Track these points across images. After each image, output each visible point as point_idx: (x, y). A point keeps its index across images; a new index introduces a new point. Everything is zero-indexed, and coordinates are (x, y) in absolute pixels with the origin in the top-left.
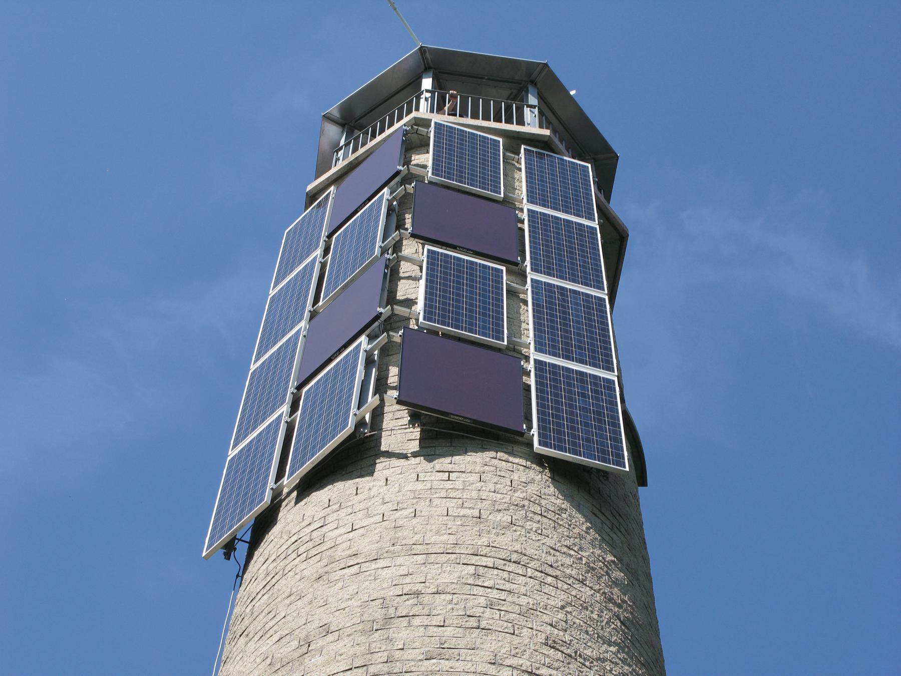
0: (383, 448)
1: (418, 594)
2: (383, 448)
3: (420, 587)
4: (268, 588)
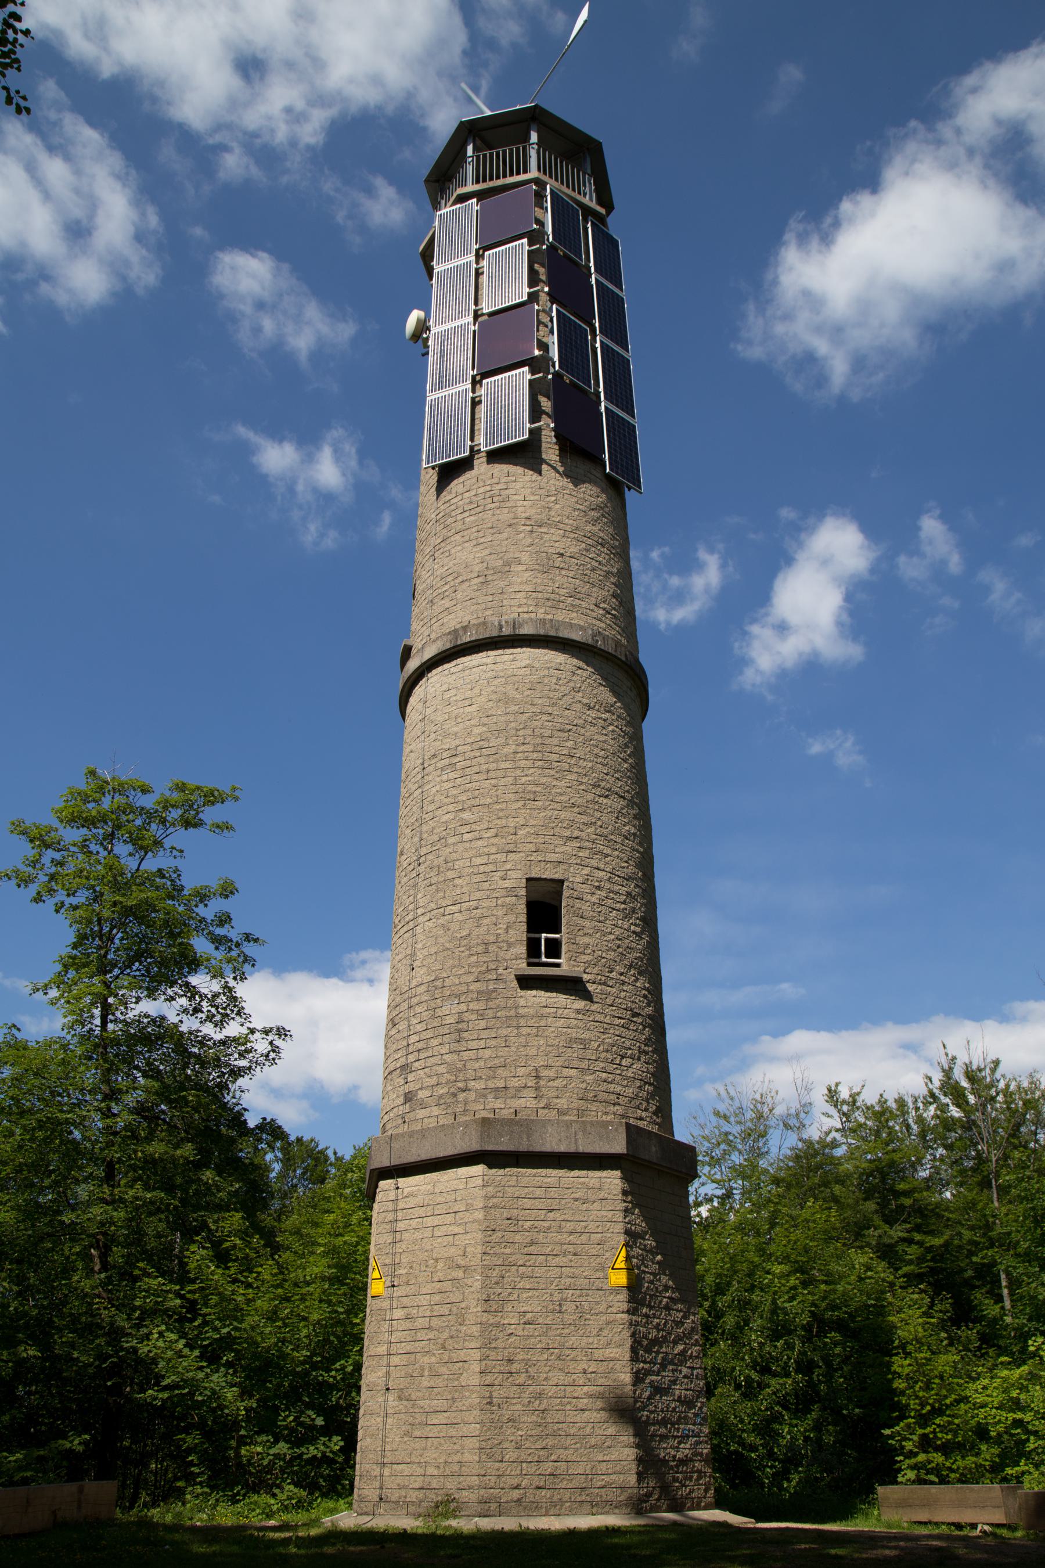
0: (612, 1180)
1: (562, 555)
2: (612, 1180)
3: (562, 551)
4: (472, 512)
